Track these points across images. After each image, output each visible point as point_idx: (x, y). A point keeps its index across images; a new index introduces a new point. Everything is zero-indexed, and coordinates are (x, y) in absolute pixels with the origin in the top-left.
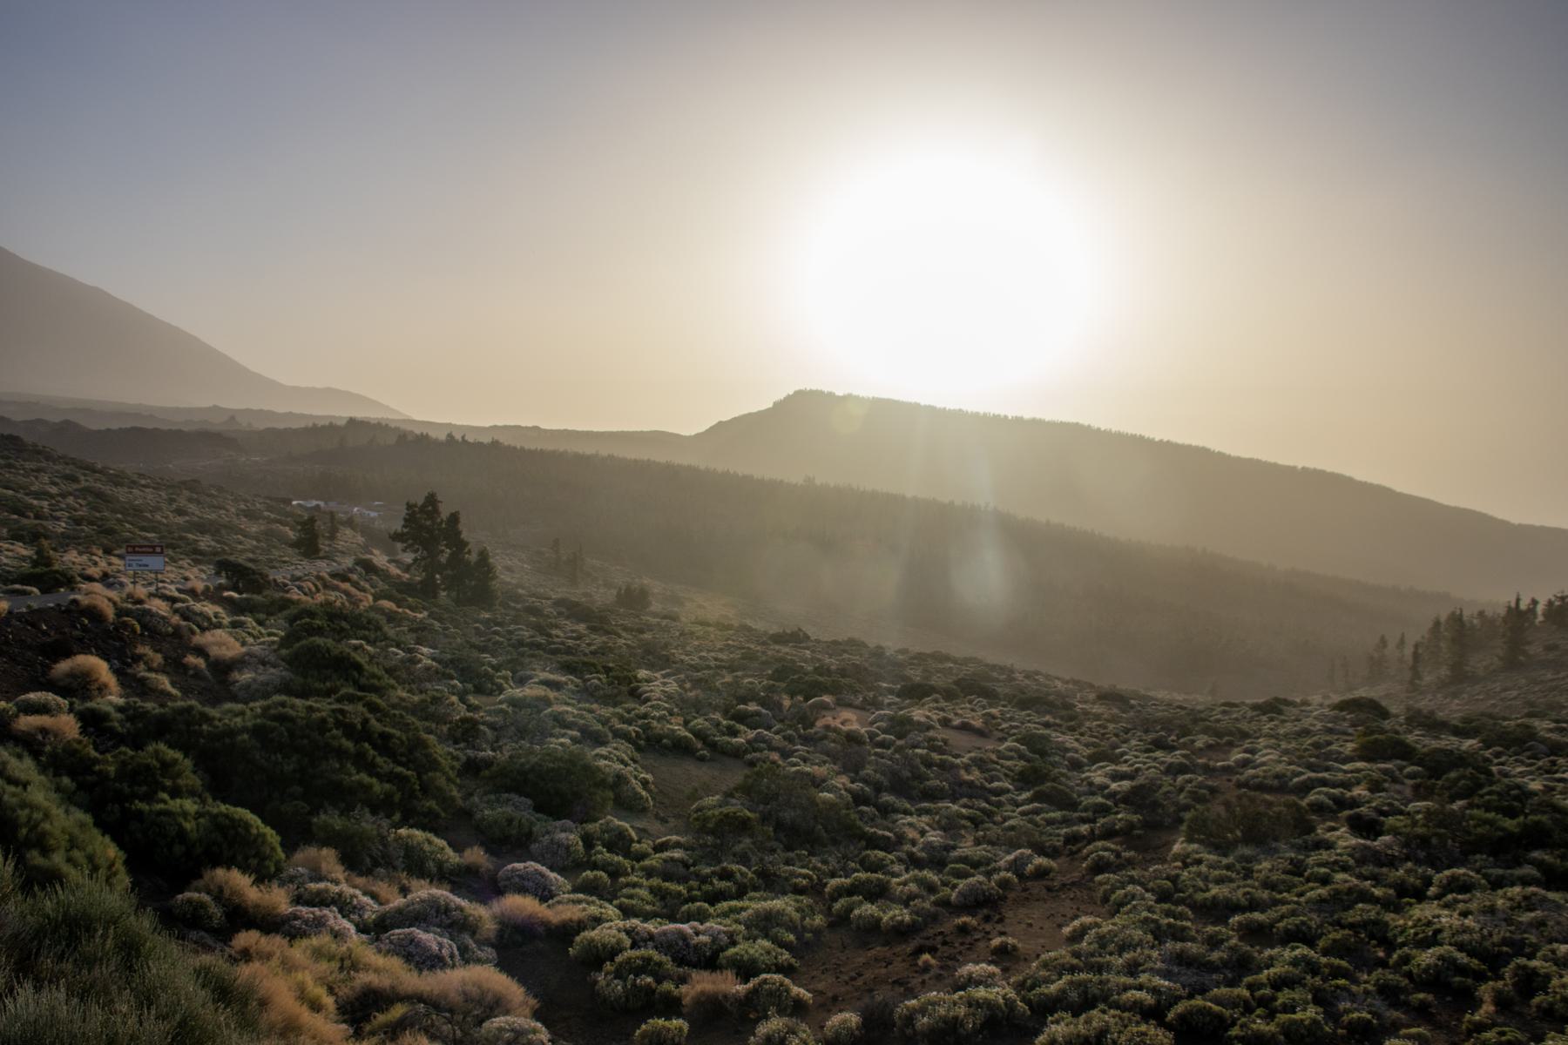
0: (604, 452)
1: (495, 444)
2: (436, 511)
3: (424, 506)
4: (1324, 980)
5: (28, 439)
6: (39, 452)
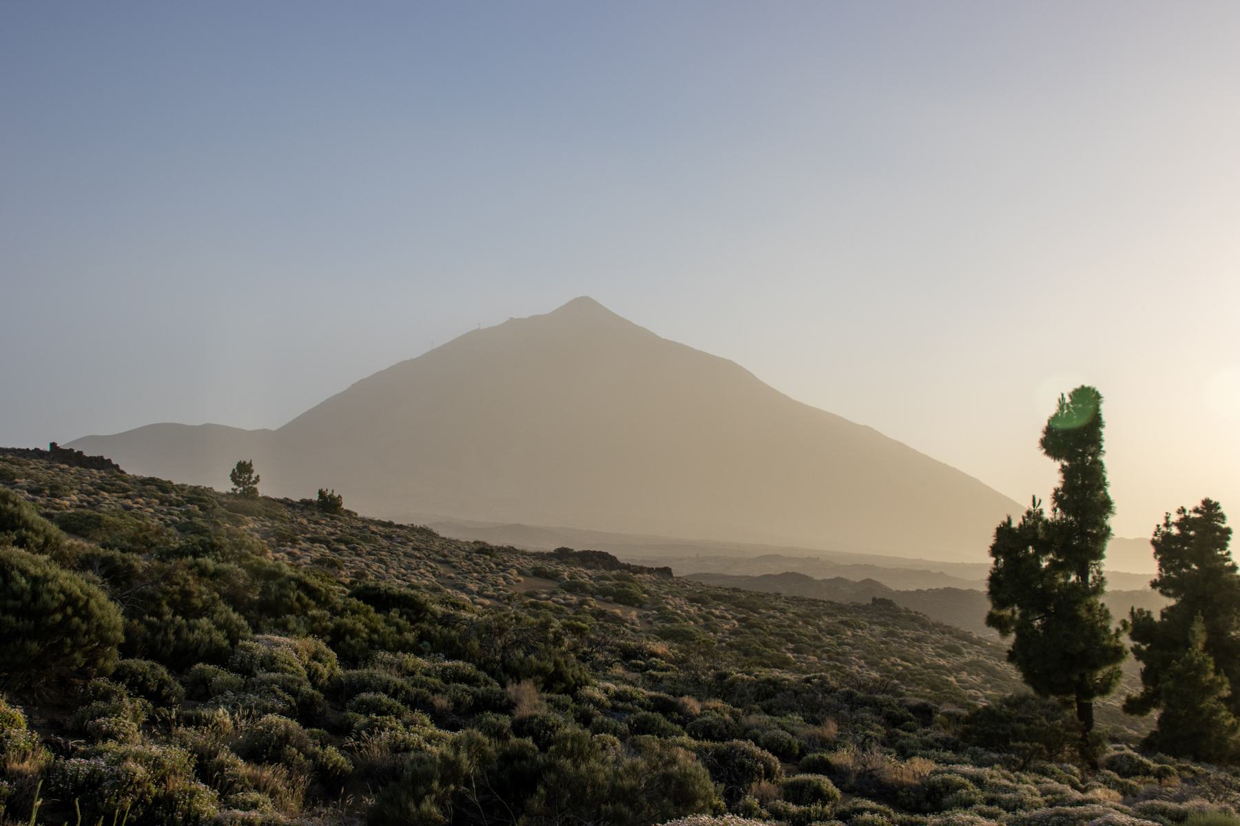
6: (914, 619)
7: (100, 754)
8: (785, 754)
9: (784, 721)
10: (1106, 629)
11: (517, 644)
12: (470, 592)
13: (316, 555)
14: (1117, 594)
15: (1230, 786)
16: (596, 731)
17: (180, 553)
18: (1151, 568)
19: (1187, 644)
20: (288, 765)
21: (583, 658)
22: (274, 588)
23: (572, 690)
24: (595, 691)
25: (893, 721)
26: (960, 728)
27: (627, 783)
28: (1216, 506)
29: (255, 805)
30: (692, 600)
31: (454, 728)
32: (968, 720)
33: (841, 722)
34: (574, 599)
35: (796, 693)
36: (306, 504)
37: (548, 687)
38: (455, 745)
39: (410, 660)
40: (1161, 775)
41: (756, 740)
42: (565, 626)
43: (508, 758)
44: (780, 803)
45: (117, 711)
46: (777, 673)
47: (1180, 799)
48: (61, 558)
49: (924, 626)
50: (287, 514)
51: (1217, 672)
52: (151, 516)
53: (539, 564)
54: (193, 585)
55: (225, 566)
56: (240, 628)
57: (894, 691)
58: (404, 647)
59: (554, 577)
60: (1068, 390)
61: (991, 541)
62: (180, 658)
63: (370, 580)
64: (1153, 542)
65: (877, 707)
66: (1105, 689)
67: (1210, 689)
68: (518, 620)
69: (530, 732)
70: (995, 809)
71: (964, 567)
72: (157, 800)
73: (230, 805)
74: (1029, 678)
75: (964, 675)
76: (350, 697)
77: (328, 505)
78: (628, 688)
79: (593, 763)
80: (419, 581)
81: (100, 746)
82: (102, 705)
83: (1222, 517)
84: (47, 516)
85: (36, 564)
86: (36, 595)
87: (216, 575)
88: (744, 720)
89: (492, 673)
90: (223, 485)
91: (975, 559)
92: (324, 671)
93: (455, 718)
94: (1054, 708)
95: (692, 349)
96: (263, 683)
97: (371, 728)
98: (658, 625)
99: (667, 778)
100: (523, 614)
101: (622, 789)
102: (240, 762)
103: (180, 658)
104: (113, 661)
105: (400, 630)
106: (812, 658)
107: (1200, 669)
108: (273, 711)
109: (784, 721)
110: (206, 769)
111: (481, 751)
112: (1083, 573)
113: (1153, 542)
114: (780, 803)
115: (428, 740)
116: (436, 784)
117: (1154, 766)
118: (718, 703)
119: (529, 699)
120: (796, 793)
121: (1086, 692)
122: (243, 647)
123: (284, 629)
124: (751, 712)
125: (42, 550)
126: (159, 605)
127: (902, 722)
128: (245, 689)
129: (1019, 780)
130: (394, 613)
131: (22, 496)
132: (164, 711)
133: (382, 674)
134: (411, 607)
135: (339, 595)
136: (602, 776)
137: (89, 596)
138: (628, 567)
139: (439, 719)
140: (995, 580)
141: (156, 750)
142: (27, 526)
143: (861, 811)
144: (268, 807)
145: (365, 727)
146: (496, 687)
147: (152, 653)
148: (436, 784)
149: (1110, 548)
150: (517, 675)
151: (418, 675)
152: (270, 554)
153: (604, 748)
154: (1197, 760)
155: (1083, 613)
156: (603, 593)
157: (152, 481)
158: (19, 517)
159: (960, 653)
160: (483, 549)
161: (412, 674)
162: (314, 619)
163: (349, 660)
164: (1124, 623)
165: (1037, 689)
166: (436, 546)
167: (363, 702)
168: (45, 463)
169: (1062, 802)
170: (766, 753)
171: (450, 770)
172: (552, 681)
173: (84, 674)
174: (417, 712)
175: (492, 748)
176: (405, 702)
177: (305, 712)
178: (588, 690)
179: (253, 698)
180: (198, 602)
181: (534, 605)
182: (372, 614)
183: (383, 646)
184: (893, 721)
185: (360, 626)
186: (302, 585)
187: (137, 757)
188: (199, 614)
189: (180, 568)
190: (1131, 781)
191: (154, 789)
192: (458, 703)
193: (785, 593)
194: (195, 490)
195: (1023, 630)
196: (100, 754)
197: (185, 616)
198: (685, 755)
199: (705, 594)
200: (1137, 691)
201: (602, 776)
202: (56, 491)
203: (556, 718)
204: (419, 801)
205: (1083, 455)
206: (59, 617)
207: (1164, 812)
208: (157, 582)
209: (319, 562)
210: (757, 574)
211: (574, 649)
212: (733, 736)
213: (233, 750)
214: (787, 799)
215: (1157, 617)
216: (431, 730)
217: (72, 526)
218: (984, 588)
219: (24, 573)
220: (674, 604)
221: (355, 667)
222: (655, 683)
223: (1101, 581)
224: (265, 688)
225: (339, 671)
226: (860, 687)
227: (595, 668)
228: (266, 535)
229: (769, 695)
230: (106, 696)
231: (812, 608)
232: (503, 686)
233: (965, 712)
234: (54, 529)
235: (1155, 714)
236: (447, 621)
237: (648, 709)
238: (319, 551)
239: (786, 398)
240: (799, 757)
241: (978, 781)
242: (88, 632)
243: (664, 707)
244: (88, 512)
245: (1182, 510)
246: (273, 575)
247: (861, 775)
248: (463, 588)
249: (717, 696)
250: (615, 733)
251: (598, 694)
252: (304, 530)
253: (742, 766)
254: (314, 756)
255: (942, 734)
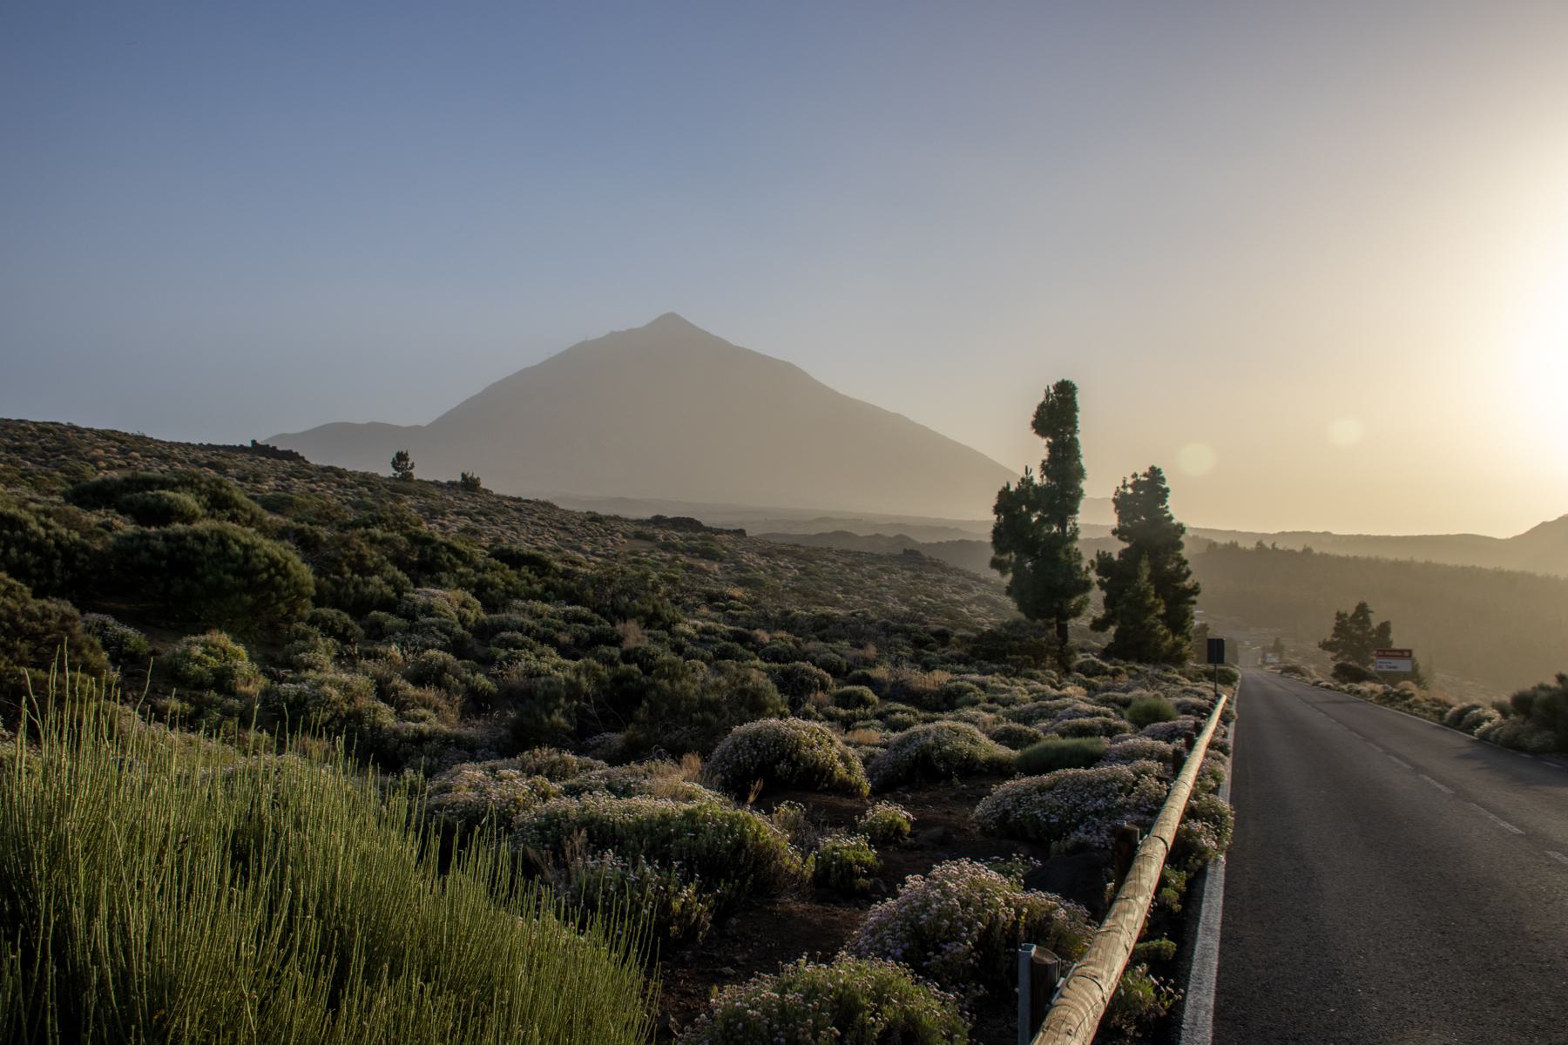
0: (1420, 558)
1: (1234, 546)
2: (1367, 621)
3: (1355, 615)
4: (503, 570)
5: (926, 554)
6: (935, 565)
7: (304, 680)
8: (835, 671)
9: (834, 646)
10: (1078, 567)
11: (623, 592)
12: (584, 552)
13: (462, 525)
14: (1087, 540)
15: (1162, 679)
16: (688, 658)
17: (355, 525)
18: (1113, 521)
19: (1136, 577)
20: (448, 689)
21: (676, 602)
22: (429, 551)
23: (667, 627)
24: (687, 627)
25: (919, 643)
26: (969, 647)
27: (712, 696)
28: (1159, 471)
29: (423, 719)
30: (762, 555)
31: (576, 658)
32: (976, 641)
33: (879, 646)
34: (668, 556)
35: (844, 625)
36: (452, 484)
37: (648, 625)
38: (577, 671)
39: (539, 606)
40: (1115, 674)
41: (813, 662)
42: (661, 577)
43: (618, 680)
44: (832, 709)
45: (314, 648)
46: (829, 610)
47: (1126, 690)
48: (264, 530)
49: (944, 570)
50: (437, 493)
51: (1156, 596)
52: (331, 496)
53: (639, 528)
54: (366, 550)
55: (390, 535)
56: (404, 583)
57: (920, 620)
58: (534, 596)
59: (652, 538)
60: (1052, 382)
61: (994, 502)
62: (360, 607)
63: (505, 544)
64: (1114, 500)
65: (907, 633)
66: (1077, 613)
67: (1151, 609)
68: (624, 573)
69: (636, 660)
70: (994, 706)
71: (973, 523)
72: (349, 716)
73: (404, 719)
74: (1023, 607)
75: (974, 607)
76: (492, 636)
77: (469, 485)
78: (712, 624)
79: (684, 681)
80: (546, 545)
81: (303, 674)
82: (302, 643)
83: (1163, 479)
84: (253, 498)
85: (246, 535)
86: (247, 559)
87: (383, 541)
88: (804, 647)
89: (604, 615)
90: (387, 472)
91: (981, 516)
92: (471, 615)
93: (575, 650)
94: (1039, 628)
95: (453, 410)
96: (425, 625)
97: (511, 660)
98: (736, 575)
99: (743, 692)
100: (627, 568)
101: (709, 701)
102: (410, 686)
103: (360, 607)
104: (308, 610)
105: (530, 583)
106: (857, 598)
107: (1145, 594)
108: (433, 647)
109: (834, 646)
110: (384, 691)
111: (597, 675)
112: (1063, 525)
113: (1114, 500)
114: (832, 709)
115: (556, 668)
116: (562, 701)
117: (1110, 668)
118: (783, 634)
119: (634, 634)
120: (844, 700)
121: (1063, 615)
122: (410, 600)
123: (438, 583)
124: (809, 640)
125: (249, 524)
126: (340, 566)
127: (925, 643)
128: (410, 630)
129: (1013, 683)
130: (525, 569)
131: (233, 483)
132: (349, 648)
133: (517, 617)
134: (538, 564)
135: (480, 556)
136: (692, 692)
137: (287, 559)
138: (710, 529)
139: (564, 651)
140: (997, 532)
141: (345, 677)
142: (237, 505)
143: (893, 712)
144: (434, 720)
145: (506, 659)
146: (608, 625)
147: (336, 604)
148: (562, 701)
149: (1082, 505)
150: (624, 615)
151: (545, 618)
152: (425, 524)
153: (694, 670)
154: (1140, 661)
155: (1063, 556)
156: (691, 551)
157: (331, 469)
158: (231, 498)
159: (970, 590)
160: (595, 518)
161: (541, 617)
162: (461, 575)
163: (490, 606)
164: (1092, 562)
165: (1027, 615)
166: (557, 516)
167: (503, 639)
168: (248, 456)
169: (1044, 698)
170: (821, 671)
171: (573, 690)
172: (652, 620)
173: (288, 621)
174: (546, 646)
175: (605, 672)
176: (536, 639)
177: (457, 648)
178: (680, 627)
179: (417, 637)
180: (370, 563)
181: (636, 561)
182: (507, 571)
183: (517, 596)
184: (919, 643)
185: (498, 580)
186: (451, 549)
187: (331, 683)
188: (372, 574)
189: (355, 536)
190: (1093, 680)
191: (346, 707)
192: (577, 639)
193: (835, 547)
194: (364, 475)
195: (1017, 569)
196: (304, 680)
197: (361, 574)
198: (758, 674)
199: (770, 550)
200: (1100, 613)
201: (692, 692)
202: (257, 478)
203: (655, 648)
204: (550, 713)
205: (1063, 434)
206: (265, 576)
207: (1115, 700)
208: (337, 548)
209: (465, 530)
210: (814, 533)
211: (669, 594)
212: (796, 659)
213: (404, 677)
214: (837, 705)
215: (1116, 557)
216: (557, 659)
217: (272, 505)
218: (989, 540)
219: (237, 542)
220: (746, 557)
221: (495, 612)
222: (733, 619)
223: (1076, 531)
224: (426, 630)
225: (483, 615)
226: (894, 618)
227: (685, 609)
228: (421, 510)
229: (825, 627)
230: (305, 637)
231: (857, 558)
232: (613, 624)
233: (974, 635)
234: (257, 508)
235: (1112, 630)
236: (567, 575)
237: (728, 640)
238: (464, 522)
239: (834, 392)
240: (847, 674)
241: (983, 686)
242: (288, 588)
243: (741, 638)
244: (283, 494)
245: (1135, 475)
246: (428, 541)
247: (894, 685)
248: (579, 549)
249: (782, 628)
250: (702, 659)
251: (689, 630)
252: (451, 505)
253: (802, 681)
254: (466, 681)
255: (956, 652)
